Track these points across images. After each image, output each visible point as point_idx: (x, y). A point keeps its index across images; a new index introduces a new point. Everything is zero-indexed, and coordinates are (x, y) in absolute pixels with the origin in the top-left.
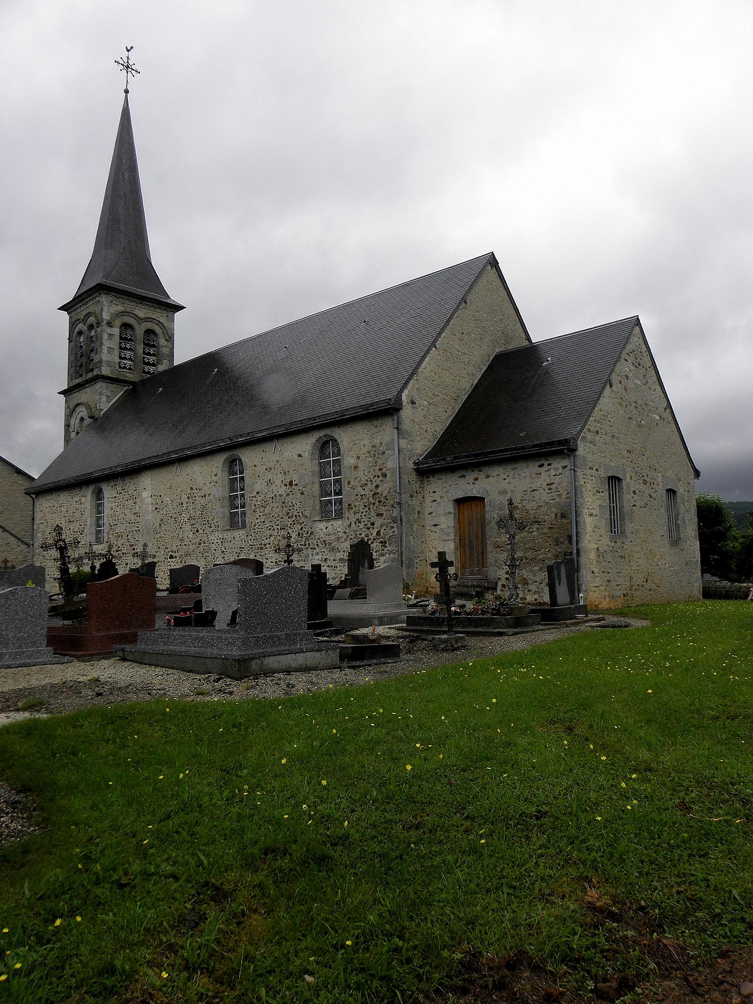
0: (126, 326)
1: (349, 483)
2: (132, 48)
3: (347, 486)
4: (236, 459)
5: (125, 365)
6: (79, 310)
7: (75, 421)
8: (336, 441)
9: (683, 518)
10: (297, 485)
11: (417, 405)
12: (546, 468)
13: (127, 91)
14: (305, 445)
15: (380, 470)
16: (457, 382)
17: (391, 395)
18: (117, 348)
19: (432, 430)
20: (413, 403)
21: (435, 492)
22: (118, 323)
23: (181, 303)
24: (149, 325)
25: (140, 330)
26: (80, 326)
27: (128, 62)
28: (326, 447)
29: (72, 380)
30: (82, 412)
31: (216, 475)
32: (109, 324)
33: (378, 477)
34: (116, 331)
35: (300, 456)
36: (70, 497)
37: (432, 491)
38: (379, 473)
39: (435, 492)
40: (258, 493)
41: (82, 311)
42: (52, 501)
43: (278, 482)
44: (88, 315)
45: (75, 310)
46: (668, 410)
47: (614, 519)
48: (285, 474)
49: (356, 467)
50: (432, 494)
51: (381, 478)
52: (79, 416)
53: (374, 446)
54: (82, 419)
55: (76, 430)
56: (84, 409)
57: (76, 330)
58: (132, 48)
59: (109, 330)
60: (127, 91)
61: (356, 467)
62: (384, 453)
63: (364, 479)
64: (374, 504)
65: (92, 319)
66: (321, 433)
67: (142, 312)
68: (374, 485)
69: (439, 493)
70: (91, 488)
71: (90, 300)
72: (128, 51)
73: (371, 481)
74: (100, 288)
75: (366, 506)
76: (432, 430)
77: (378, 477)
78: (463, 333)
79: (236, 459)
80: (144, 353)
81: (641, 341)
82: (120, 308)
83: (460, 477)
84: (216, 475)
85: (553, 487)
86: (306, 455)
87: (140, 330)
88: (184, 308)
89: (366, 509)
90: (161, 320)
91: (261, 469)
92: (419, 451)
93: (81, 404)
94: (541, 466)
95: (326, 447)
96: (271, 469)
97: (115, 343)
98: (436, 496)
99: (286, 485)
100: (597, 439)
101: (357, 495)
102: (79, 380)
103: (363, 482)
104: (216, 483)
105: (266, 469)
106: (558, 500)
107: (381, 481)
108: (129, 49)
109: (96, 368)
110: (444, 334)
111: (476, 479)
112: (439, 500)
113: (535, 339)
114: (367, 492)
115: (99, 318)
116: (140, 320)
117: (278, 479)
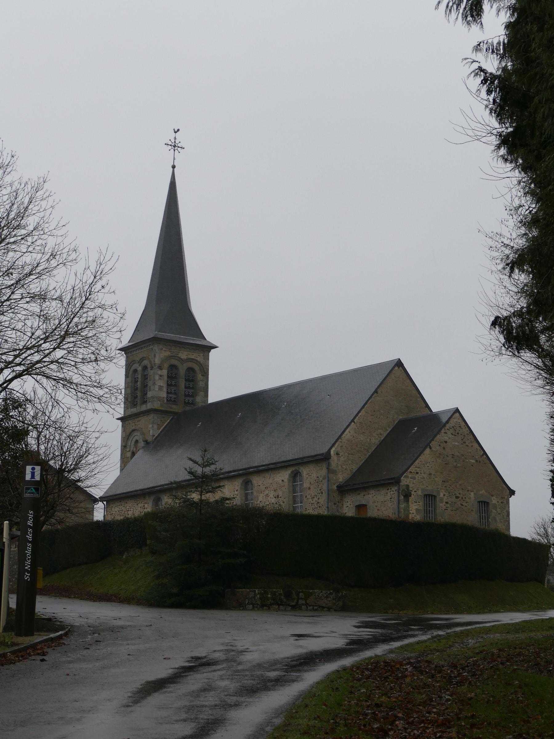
0: (172, 367)
1: (306, 497)
2: (178, 130)
3: (305, 498)
4: (249, 481)
5: (171, 398)
6: (135, 353)
7: (131, 443)
8: (301, 473)
9: (495, 519)
10: (281, 497)
11: (340, 455)
12: (389, 491)
13: (174, 167)
14: (284, 476)
15: (320, 490)
16: (368, 440)
17: (324, 450)
18: (165, 386)
19: (350, 468)
20: (338, 454)
21: (348, 502)
22: (166, 365)
23: (218, 346)
24: (190, 365)
25: (182, 371)
26: (136, 366)
27: (175, 142)
28: (295, 476)
29: (128, 408)
30: (137, 436)
31: (237, 491)
32: (160, 368)
33: (319, 494)
34: (165, 372)
35: (283, 481)
36: (136, 504)
37: (346, 501)
38: (320, 492)
39: (348, 502)
40: (261, 502)
41: (138, 355)
42: (121, 507)
43: (271, 496)
44: (142, 360)
45: (131, 352)
46: (485, 456)
47: (483, 519)
48: (275, 490)
49: (309, 488)
50: (346, 503)
51: (320, 494)
52: (134, 440)
53: (318, 477)
54: (137, 442)
55: (131, 450)
56: (139, 434)
57: (132, 369)
58: (178, 130)
59: (160, 372)
60: (174, 167)
61: (309, 488)
62: (322, 481)
63: (313, 494)
64: (317, 508)
65: (145, 362)
66: (293, 469)
67: (184, 355)
68: (318, 498)
69: (349, 503)
70: (152, 498)
71: (145, 347)
72: (175, 132)
73: (316, 496)
74: (155, 340)
75: (313, 509)
76: (350, 468)
77: (319, 494)
78: (374, 411)
79: (249, 481)
80: (186, 387)
81: (460, 420)
82: (168, 353)
83: (358, 494)
84: (237, 491)
85: (392, 499)
86: (286, 480)
87: (182, 371)
88: (216, 347)
89: (314, 511)
90: (198, 359)
91: (262, 488)
92: (341, 480)
93: (136, 430)
94: (388, 489)
95: (295, 476)
96: (267, 488)
97: (162, 383)
98: (348, 504)
99: (275, 498)
100: (416, 477)
101: (310, 503)
102: (134, 410)
103: (313, 496)
104: (237, 495)
105: (265, 488)
106: (393, 506)
107: (321, 496)
108: (176, 131)
109: (150, 402)
110: (360, 414)
111: (364, 495)
112: (349, 506)
113: (435, 409)
114: (314, 502)
115: (153, 362)
116: (182, 361)
117: (272, 494)
